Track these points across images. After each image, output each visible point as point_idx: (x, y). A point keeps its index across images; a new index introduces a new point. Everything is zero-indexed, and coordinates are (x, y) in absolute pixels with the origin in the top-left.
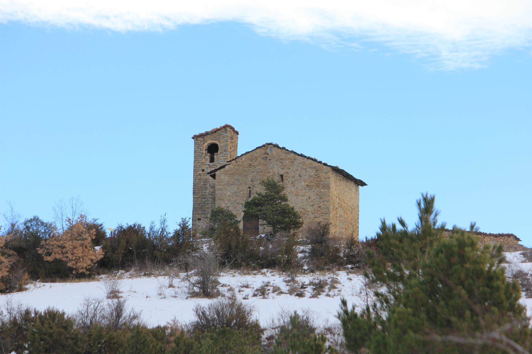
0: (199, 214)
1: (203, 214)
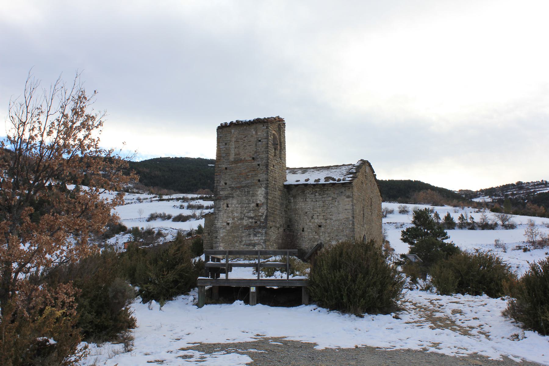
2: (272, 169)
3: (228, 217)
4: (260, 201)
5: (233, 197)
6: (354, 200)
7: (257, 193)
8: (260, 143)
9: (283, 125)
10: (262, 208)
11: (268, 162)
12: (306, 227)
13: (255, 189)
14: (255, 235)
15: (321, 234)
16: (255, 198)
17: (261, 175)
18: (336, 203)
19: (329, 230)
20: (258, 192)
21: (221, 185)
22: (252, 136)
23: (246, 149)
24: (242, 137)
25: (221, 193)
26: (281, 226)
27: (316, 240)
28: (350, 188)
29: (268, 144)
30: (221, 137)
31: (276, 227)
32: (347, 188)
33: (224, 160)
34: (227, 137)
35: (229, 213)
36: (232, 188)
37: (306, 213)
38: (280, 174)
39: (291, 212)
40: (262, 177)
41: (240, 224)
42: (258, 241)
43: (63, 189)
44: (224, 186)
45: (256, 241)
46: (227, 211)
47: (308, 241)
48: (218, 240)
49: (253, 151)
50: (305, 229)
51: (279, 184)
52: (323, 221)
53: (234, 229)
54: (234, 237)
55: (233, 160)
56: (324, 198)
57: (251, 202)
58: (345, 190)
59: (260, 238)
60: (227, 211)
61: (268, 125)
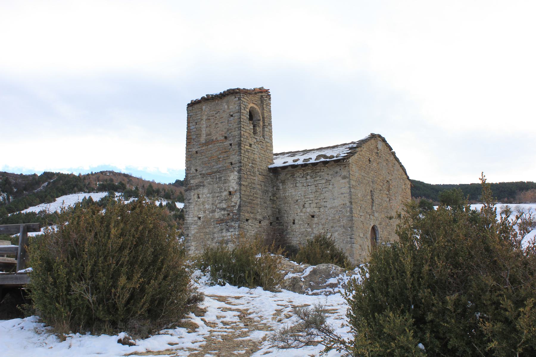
0: (248, 212)
1: (253, 213)
2: (247, 149)
4: (233, 188)
5: (204, 186)
6: (352, 181)
9: (267, 97)
10: (235, 197)
11: (241, 140)
12: (297, 218)
13: (227, 175)
14: (228, 230)
15: (314, 226)
16: (227, 184)
17: (233, 156)
18: (331, 186)
19: (323, 221)
21: (191, 172)
22: (224, 111)
23: (218, 127)
24: (213, 114)
25: (192, 181)
26: (264, 218)
27: (308, 234)
28: (346, 167)
29: (240, 118)
30: (191, 115)
31: (256, 219)
32: (342, 167)
33: (195, 143)
34: (198, 115)
35: (200, 205)
36: (203, 175)
37: (297, 201)
38: (262, 155)
39: (280, 201)
40: (234, 158)
41: (211, 218)
43: (172, 207)
44: (195, 173)
45: (229, 237)
46: (198, 203)
47: (300, 236)
48: (189, 238)
49: (225, 128)
50: (296, 221)
51: (259, 167)
52: (316, 210)
53: (205, 224)
54: (206, 234)
55: (204, 142)
57: (223, 191)
58: (340, 169)
59: (233, 233)
60: (198, 203)
61: (240, 95)
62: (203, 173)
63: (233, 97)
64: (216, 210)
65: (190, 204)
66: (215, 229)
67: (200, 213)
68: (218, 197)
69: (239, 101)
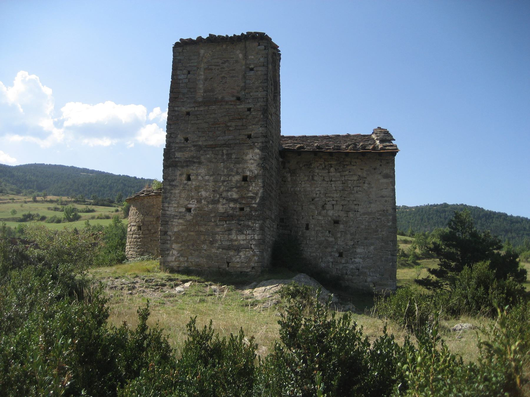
3: (189, 198)
4: (251, 171)
5: (200, 163)
7: (245, 158)
8: (252, 73)
10: (254, 185)
12: (312, 222)
14: (241, 232)
15: (339, 235)
16: (241, 165)
17: (253, 126)
18: (366, 185)
20: (248, 156)
21: (178, 141)
23: (226, 82)
24: (218, 62)
25: (178, 155)
30: (180, 60)
33: (185, 100)
34: (192, 61)
36: (199, 148)
37: (313, 200)
41: (211, 211)
42: (245, 242)
45: (242, 242)
46: (187, 187)
47: (317, 246)
48: (169, 238)
49: (238, 86)
50: (311, 226)
52: (342, 214)
54: (199, 233)
55: (200, 100)
56: (345, 176)
57: (233, 173)
58: (381, 165)
59: (249, 237)
60: (187, 187)
62: (200, 145)
63: (256, 44)
64: (221, 200)
65: (173, 188)
66: (218, 228)
67: (191, 202)
68: (224, 181)
69: (265, 51)
